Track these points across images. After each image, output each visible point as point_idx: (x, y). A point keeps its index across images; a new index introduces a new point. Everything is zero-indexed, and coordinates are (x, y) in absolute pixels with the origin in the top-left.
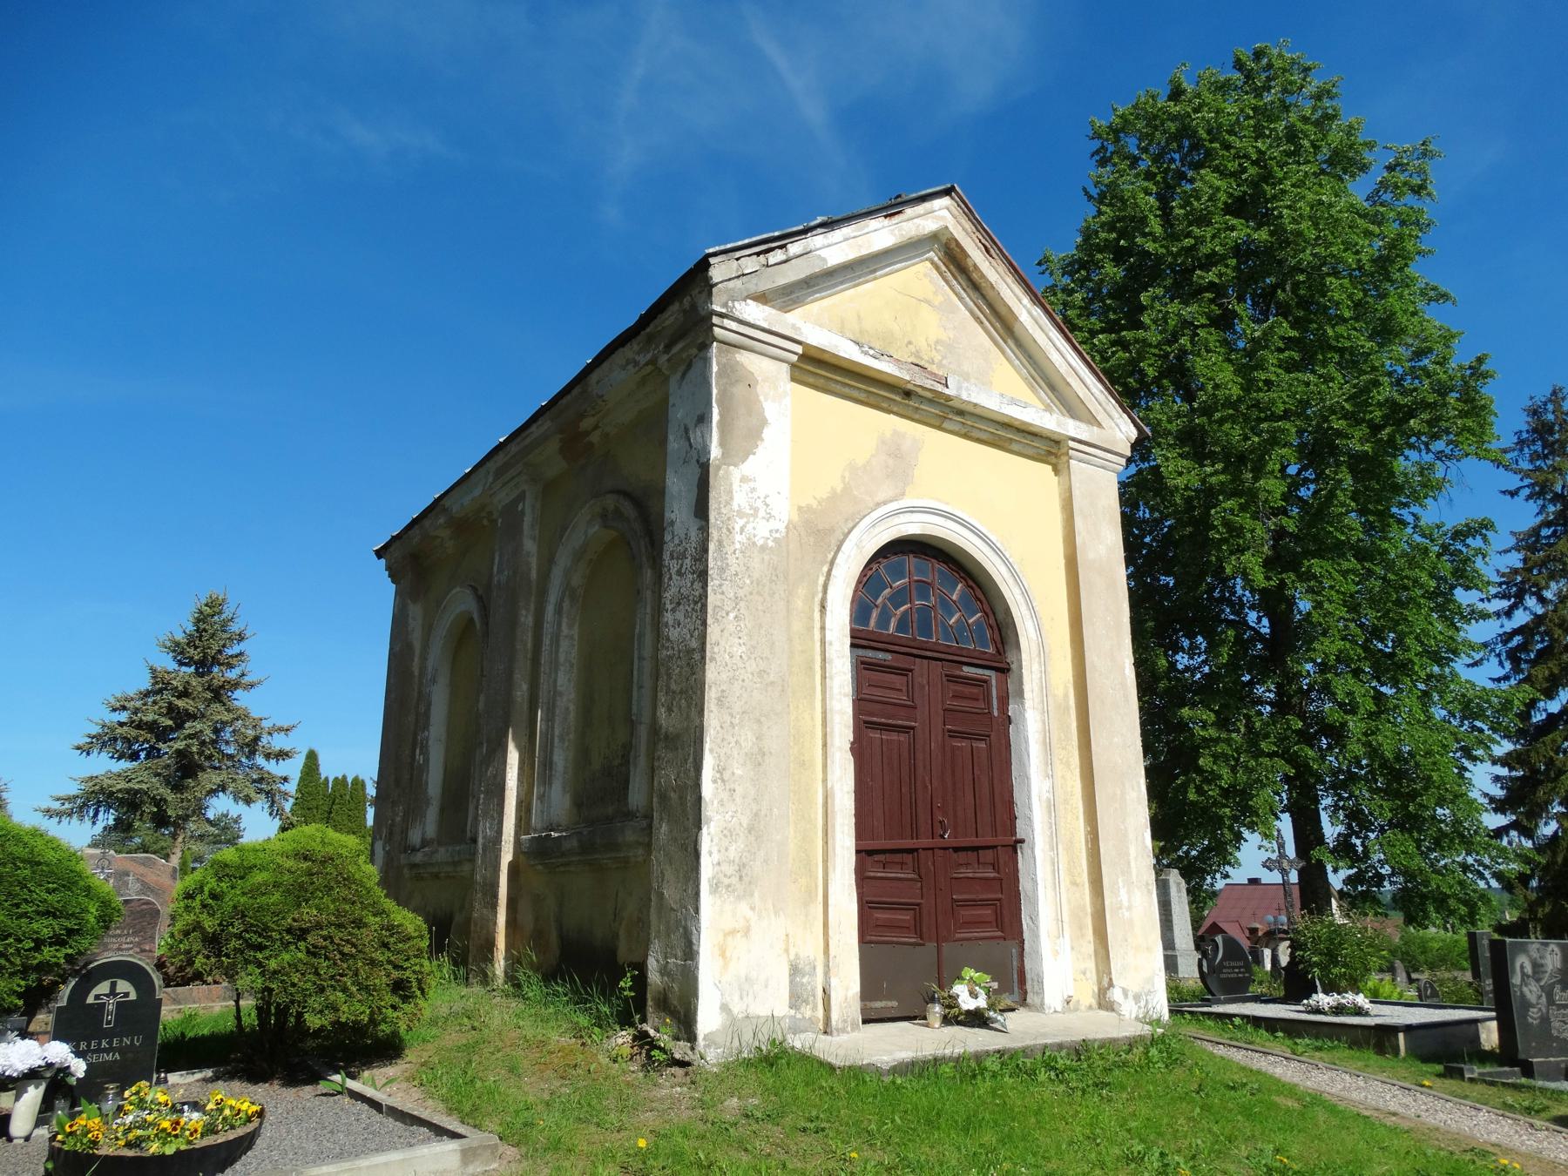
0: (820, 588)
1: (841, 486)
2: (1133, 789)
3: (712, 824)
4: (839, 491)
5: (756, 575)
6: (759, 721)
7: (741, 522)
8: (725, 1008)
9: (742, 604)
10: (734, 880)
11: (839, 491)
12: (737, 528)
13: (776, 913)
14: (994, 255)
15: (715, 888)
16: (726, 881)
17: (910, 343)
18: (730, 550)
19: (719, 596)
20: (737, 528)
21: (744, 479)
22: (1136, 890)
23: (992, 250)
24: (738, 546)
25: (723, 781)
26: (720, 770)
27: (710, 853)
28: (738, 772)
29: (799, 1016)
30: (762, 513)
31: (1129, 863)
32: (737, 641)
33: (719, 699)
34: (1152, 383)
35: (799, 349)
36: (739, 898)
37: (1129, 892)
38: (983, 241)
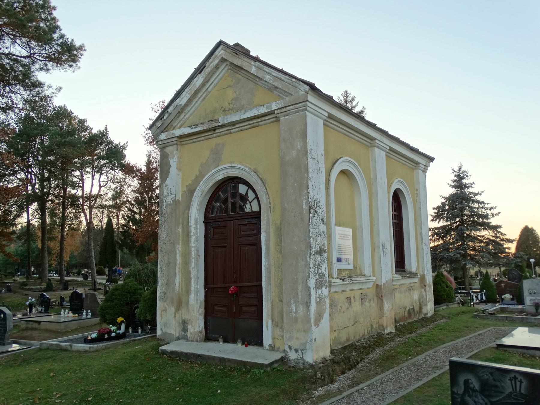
0: (267, 188)
1: (199, 173)
2: (303, 260)
3: (159, 283)
4: (198, 175)
5: (168, 213)
6: (169, 254)
7: (165, 199)
8: (161, 329)
9: (166, 222)
10: (164, 297)
11: (198, 175)
12: (165, 201)
13: (172, 306)
14: (239, 54)
15: (160, 299)
16: (162, 297)
17: (222, 107)
18: (163, 208)
19: (161, 222)
20: (165, 201)
21: (166, 186)
22: (300, 305)
23: (237, 53)
24: (165, 206)
25: (162, 271)
26: (161, 269)
27: (159, 290)
28: (164, 269)
29: (185, 335)
30: (170, 194)
31: (297, 293)
32: (164, 233)
33: (161, 250)
34: (46, 186)
35: (176, 139)
36: (164, 302)
37: (296, 306)
38: (234, 52)
